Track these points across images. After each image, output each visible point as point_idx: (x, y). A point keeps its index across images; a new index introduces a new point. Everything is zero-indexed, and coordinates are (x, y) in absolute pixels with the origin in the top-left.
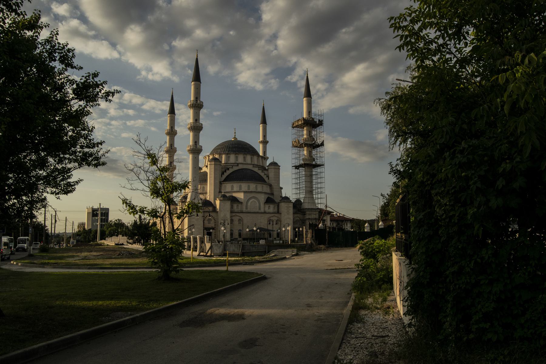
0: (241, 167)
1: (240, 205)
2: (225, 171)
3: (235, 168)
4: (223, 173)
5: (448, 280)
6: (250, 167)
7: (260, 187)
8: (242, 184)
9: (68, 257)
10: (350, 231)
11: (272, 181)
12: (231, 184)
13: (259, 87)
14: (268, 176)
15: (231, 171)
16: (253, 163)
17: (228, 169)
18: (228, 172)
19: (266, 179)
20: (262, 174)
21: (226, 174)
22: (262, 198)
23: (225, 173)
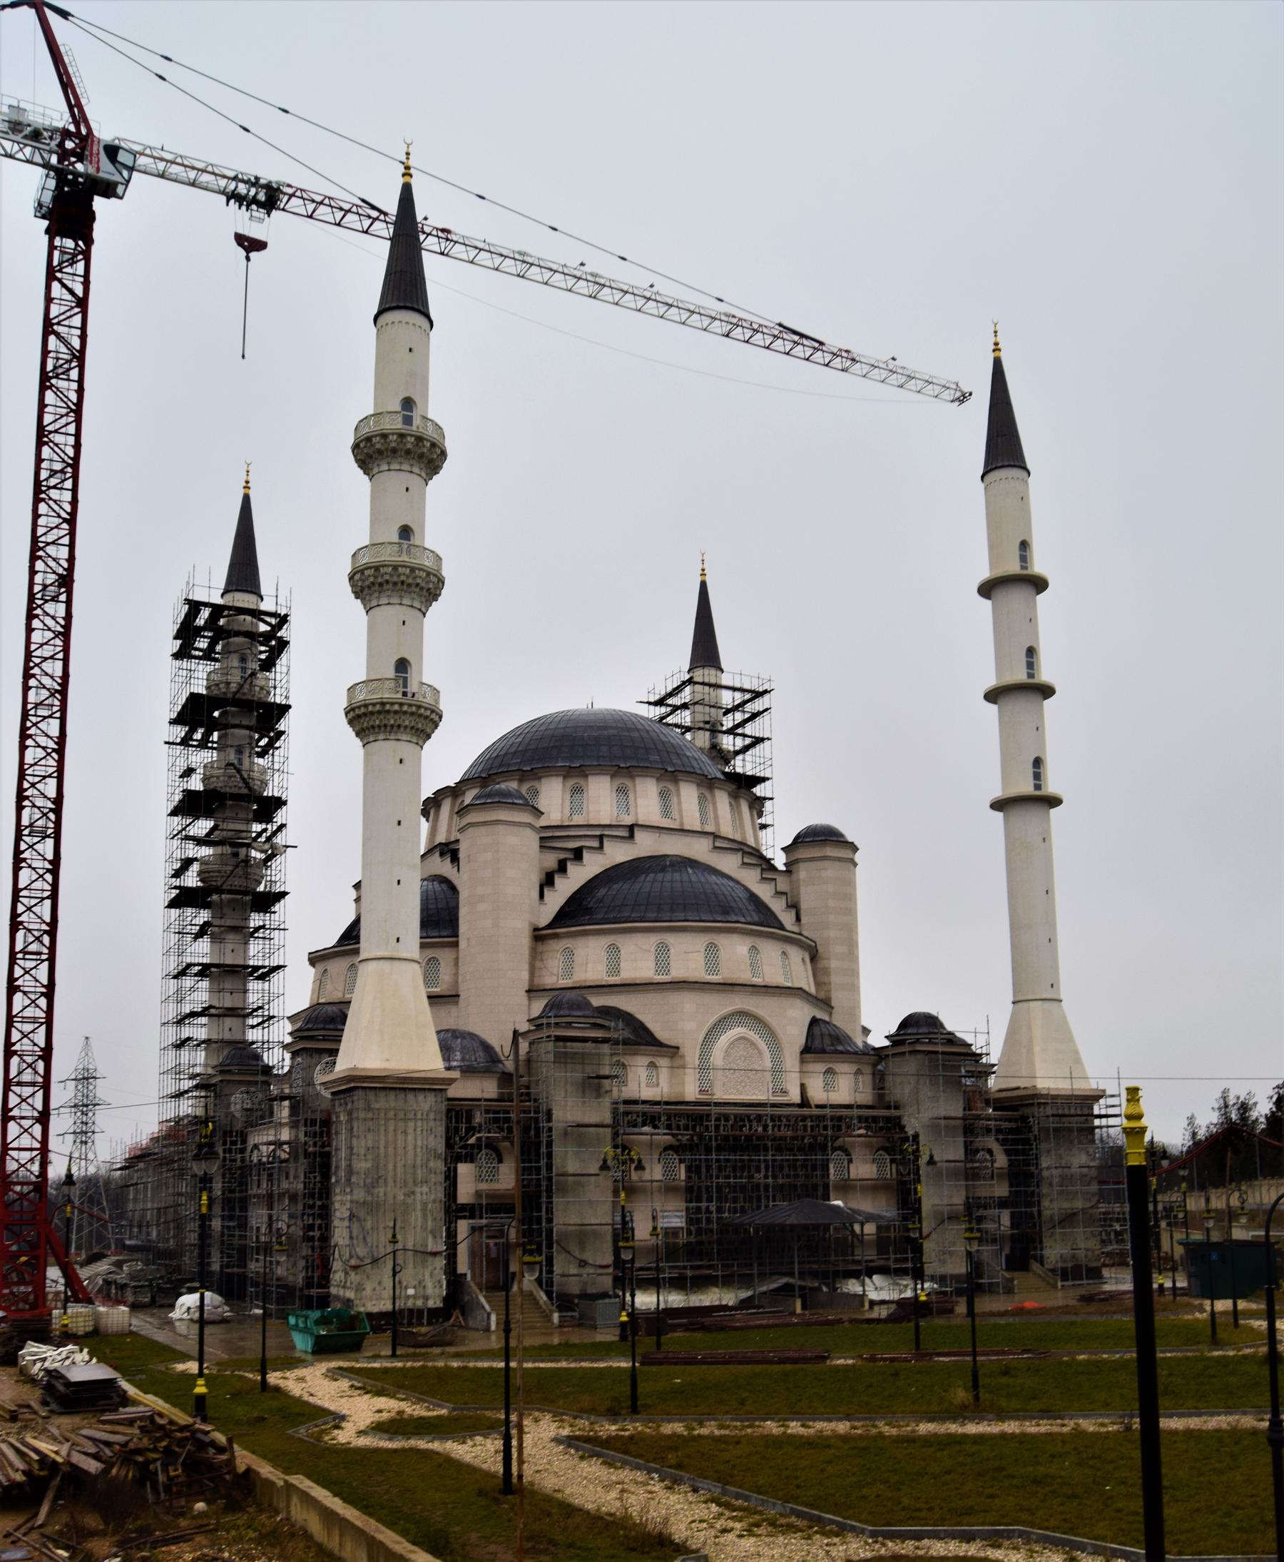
0: (645, 845)
1: (663, 1062)
2: (562, 868)
3: (617, 853)
4: (548, 881)
5: (694, 1424)
6: (699, 850)
7: (779, 964)
8: (672, 940)
9: (1004, 1314)
10: (1151, 1284)
11: (828, 938)
12: (604, 941)
13: (199, 884)
14: (794, 906)
15: (592, 866)
16: (710, 828)
17: (578, 855)
18: (578, 876)
19: (787, 919)
20: (765, 892)
21: (566, 887)
22: (793, 1022)
23: (558, 880)
